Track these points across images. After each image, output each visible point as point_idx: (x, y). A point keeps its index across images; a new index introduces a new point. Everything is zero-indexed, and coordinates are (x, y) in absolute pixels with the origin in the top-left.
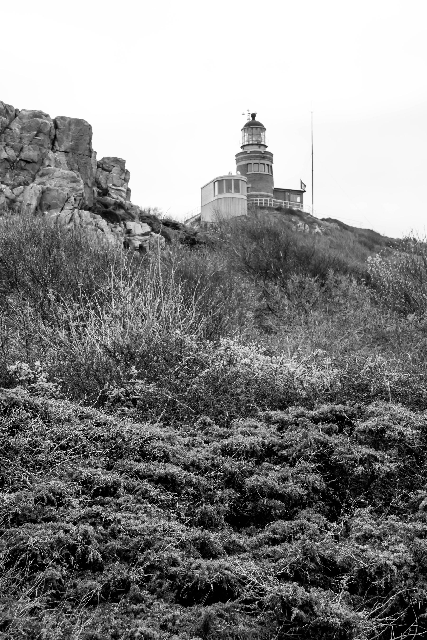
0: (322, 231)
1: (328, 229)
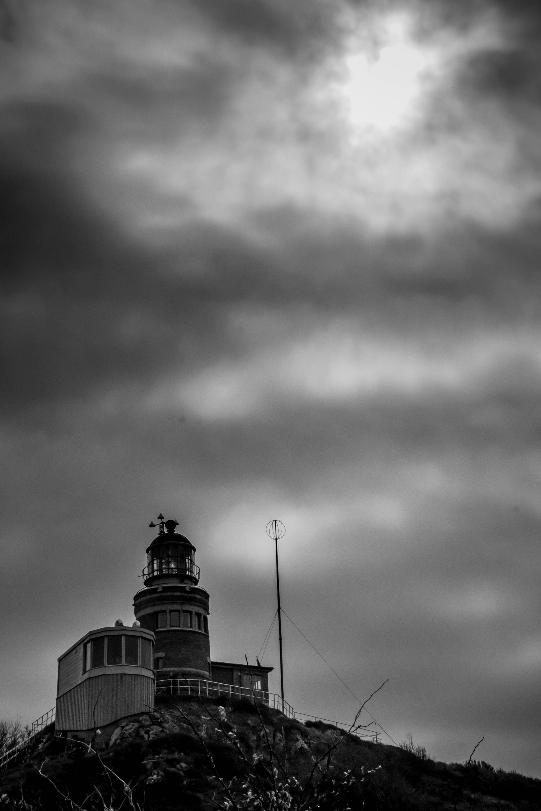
0: (309, 746)
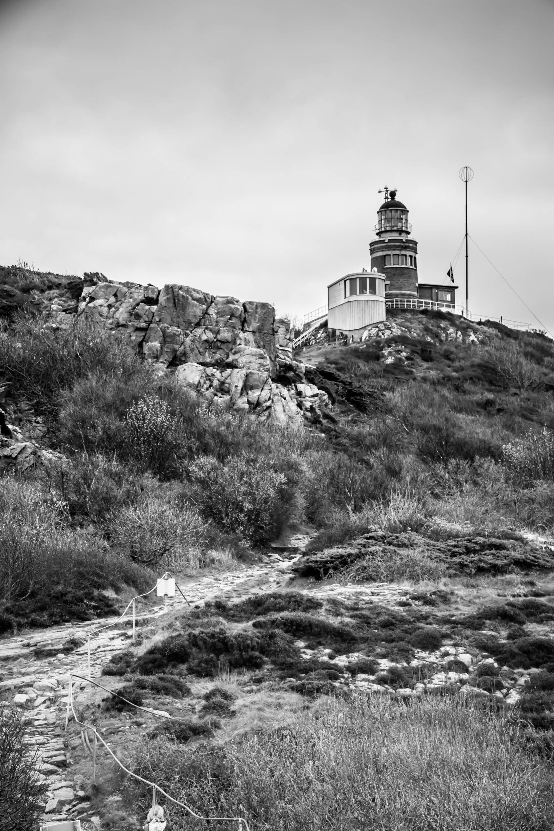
0: (478, 339)
1: (486, 336)
